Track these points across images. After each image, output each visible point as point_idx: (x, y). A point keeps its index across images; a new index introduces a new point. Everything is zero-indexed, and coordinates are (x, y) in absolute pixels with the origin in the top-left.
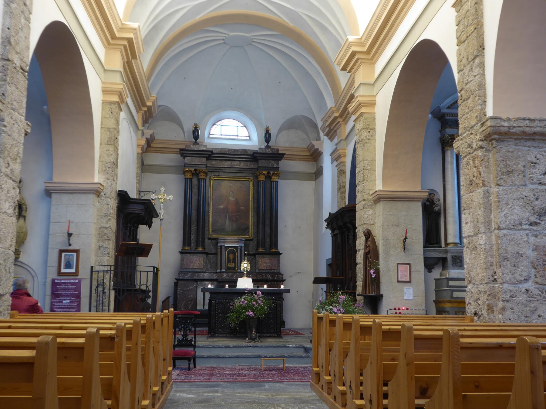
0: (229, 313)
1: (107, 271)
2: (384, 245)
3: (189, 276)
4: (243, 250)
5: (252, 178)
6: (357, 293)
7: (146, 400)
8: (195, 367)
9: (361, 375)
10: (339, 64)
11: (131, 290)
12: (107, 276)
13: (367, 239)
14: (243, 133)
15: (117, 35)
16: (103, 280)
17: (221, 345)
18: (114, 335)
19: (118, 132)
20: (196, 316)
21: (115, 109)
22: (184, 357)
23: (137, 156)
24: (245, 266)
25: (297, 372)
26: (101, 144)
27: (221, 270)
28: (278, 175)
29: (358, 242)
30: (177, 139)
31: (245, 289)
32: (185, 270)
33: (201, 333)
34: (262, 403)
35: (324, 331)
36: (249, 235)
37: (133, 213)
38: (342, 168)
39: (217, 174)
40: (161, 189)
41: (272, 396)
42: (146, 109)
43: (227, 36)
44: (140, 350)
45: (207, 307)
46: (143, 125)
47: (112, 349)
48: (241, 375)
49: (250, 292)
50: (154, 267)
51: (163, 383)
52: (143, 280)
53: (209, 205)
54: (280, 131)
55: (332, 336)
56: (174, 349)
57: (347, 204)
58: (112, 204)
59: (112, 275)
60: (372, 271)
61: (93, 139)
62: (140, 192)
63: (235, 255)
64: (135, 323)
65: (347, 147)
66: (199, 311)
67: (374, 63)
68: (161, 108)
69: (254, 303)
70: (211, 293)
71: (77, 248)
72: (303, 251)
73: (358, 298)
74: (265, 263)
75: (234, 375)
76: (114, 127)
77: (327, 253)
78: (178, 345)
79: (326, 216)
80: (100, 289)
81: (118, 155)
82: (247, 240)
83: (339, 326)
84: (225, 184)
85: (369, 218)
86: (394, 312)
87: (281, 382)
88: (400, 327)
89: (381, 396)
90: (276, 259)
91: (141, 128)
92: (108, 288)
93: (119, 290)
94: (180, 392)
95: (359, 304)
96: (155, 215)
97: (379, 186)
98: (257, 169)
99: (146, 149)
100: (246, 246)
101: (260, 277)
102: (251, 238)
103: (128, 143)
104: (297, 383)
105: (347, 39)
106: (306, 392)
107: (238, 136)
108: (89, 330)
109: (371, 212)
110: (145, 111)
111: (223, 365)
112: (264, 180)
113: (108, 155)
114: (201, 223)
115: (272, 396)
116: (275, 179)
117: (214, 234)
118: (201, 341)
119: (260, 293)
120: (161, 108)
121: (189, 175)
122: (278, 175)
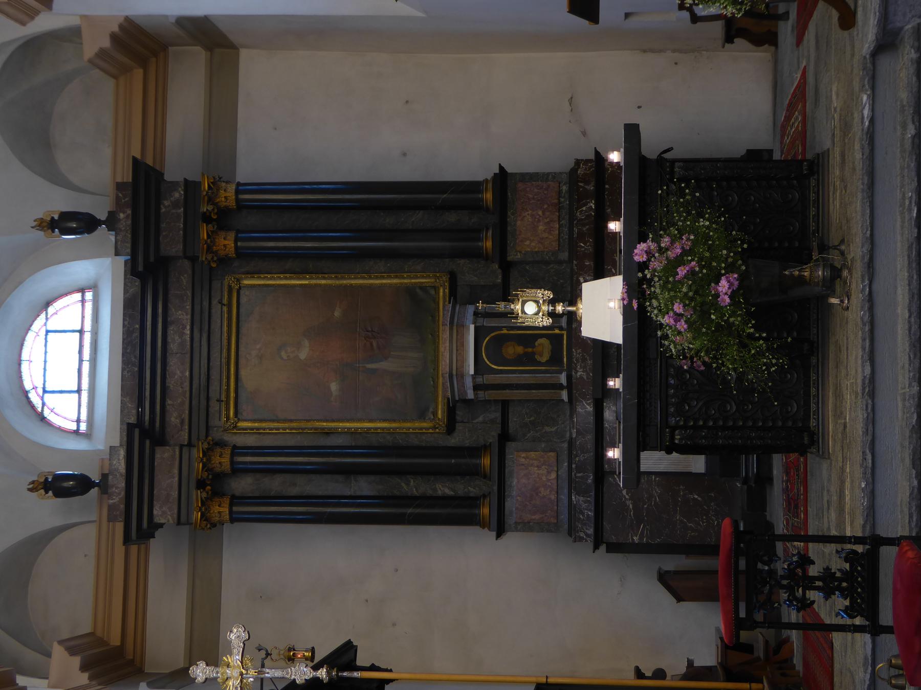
3: (585, 505)
5: (229, 280)
14: (69, 312)
17: (861, 415)
27: (561, 387)
28: (215, 184)
31: (627, 311)
32: (564, 517)
36: (436, 289)
40: (200, 678)
49: (637, 291)
53: (328, 433)
54: (56, 178)
69: (682, 271)
70: (643, 445)
78: (872, 613)
82: (453, 293)
84: (251, 377)
90: (520, 186)
98: (193, 259)
101: (586, 247)
102: (445, 278)
107: (81, 332)
112: (232, 235)
114: (394, 460)
117: (435, 414)
119: (642, 246)
121: (220, 509)
122: (215, 184)
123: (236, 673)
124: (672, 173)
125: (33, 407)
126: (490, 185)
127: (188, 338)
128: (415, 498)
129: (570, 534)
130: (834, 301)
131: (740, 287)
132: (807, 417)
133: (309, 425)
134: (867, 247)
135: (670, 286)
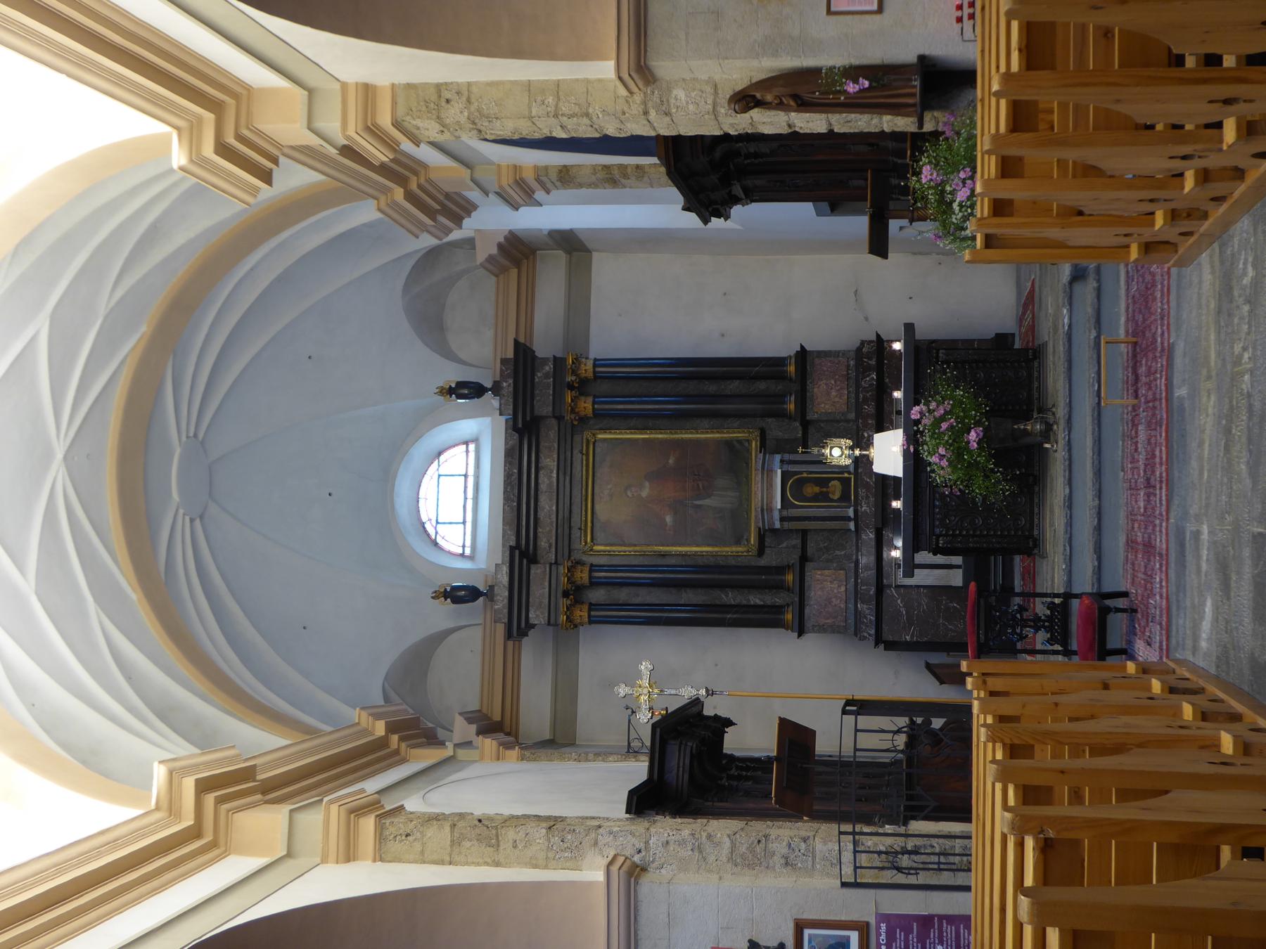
0: (973, 499)
1: (855, 843)
2: (775, 54)
3: (867, 610)
4: (792, 457)
5: (587, 434)
6: (913, 128)
7: (1219, 739)
8: (1125, 594)
9: (1152, 127)
10: (254, 191)
11: (909, 776)
12: (869, 842)
13: (759, 104)
14: (457, 460)
15: (188, 821)
16: (880, 853)
18: (1036, 840)
19: (462, 816)
20: (981, 592)
21: (396, 825)
22: (1098, 627)
23: (529, 760)
24: (838, 453)
25: (1143, 302)
26: (497, 864)
27: (849, 519)
28: (577, 360)
29: (767, 130)
30: (479, 647)
31: (906, 454)
32: (851, 621)
33: (1030, 575)
34: (1231, 408)
35: (1027, 232)
36: (749, 441)
37: (691, 771)
38: (553, 175)
39: (576, 533)
40: (622, 694)
41: (1209, 378)
42: (395, 738)
43: (181, 511)
44: (1079, 763)
45: (958, 560)
46: (442, 744)
47: (1076, 844)
48: (1150, 465)
49: (913, 439)
50: (844, 712)
51: (1172, 690)
52: (882, 739)
53: (663, 555)
55: (1038, 209)
56: (1075, 653)
57: (655, 160)
58: (666, 831)
59: (866, 829)
60: (851, 88)
61: (482, 887)
62: (630, 752)
63: (808, 480)
64: (1004, 776)
65: (493, 164)
66: (966, 580)
67: (248, 88)
68: (392, 695)
69: (944, 426)
71: (791, 925)
72: (792, 281)
73: (928, 127)
74: (828, 394)
75: (1148, 485)
76: (447, 829)
77: (798, 215)
78: (1065, 641)
79: (692, 220)
80: (905, 861)
81: (526, 817)
83: (1012, 190)
85: (697, 96)
86: (967, 24)
87: (1169, 352)
88: (1015, 25)
89: (1213, 72)
91: (449, 751)
92: (903, 839)
93: (907, 808)
94: (1196, 638)
95: (945, 124)
96: (695, 710)
97: (605, 69)
98: (560, 418)
99: (508, 734)
100: (782, 447)
101: (869, 408)
102: (757, 433)
103: (492, 786)
104: (1173, 304)
105: (182, 169)
106: (1200, 282)
107: (466, 476)
108: (1024, 915)
109: (679, 93)
110: (401, 739)
111: (1122, 514)
112: (590, 399)
113: (528, 844)
114: (716, 576)
115: (1209, 378)
116: (587, 369)
117: (748, 540)
118: (1052, 577)
119: (917, 408)
120: (392, 695)
121: (581, 613)
122: (577, 360)
123: (645, 691)
124: (937, 357)
125: (428, 535)
126: (793, 360)
127: (555, 480)
128: (731, 606)
129: (856, 635)
130: (1047, 446)
131: (984, 436)
132: (1032, 528)
133: (649, 548)
134: (1067, 409)
135: (936, 435)
